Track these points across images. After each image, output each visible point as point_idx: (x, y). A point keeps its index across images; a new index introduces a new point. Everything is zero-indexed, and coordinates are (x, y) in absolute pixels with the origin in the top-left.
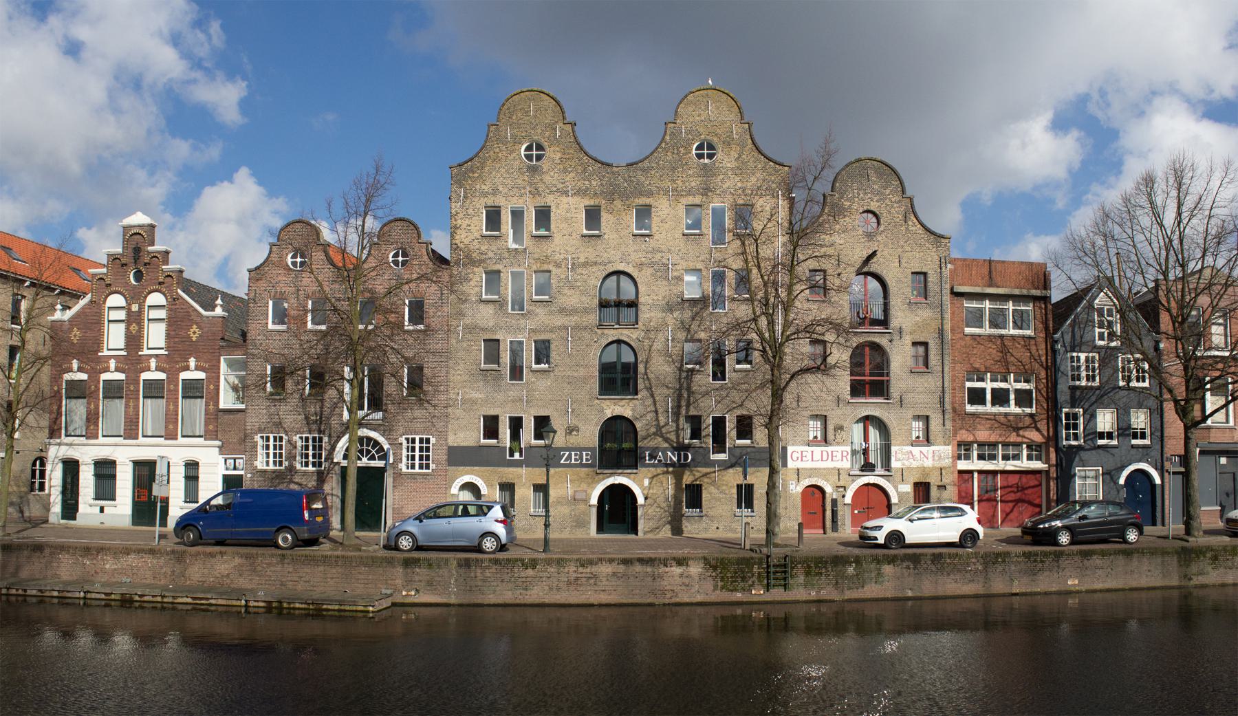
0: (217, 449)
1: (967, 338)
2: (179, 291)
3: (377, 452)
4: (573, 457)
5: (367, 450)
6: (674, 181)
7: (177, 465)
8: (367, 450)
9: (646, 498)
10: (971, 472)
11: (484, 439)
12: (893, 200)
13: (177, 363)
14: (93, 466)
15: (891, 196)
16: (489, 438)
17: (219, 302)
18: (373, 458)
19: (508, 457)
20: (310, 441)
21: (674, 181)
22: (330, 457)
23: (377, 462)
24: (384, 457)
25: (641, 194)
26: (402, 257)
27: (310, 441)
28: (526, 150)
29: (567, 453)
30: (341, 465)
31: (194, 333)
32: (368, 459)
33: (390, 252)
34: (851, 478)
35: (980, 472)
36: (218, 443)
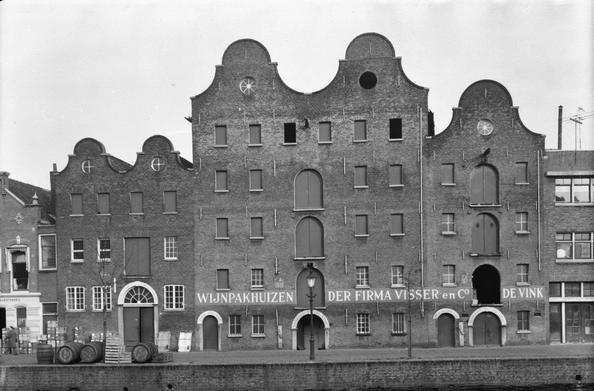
0: (38, 298)
1: (557, 209)
2: (6, 189)
3: (147, 297)
4: (280, 296)
5: (145, 300)
6: (346, 103)
7: (11, 309)
8: (140, 296)
9: (330, 324)
10: (560, 303)
11: (75, 258)
12: (504, 110)
13: (7, 239)
14: (573, 149)
15: (502, 108)
16: (77, 258)
17: (35, 196)
18: (144, 301)
19: (183, 286)
20: (102, 290)
21: (346, 103)
22: (115, 299)
23: (147, 303)
24: (152, 300)
25: (324, 114)
26: (160, 163)
27: (102, 290)
28: (242, 85)
29: (276, 293)
30: (124, 306)
31: (19, 218)
32: (142, 302)
33: (152, 160)
34: (472, 308)
35: (566, 303)
36: (39, 294)
